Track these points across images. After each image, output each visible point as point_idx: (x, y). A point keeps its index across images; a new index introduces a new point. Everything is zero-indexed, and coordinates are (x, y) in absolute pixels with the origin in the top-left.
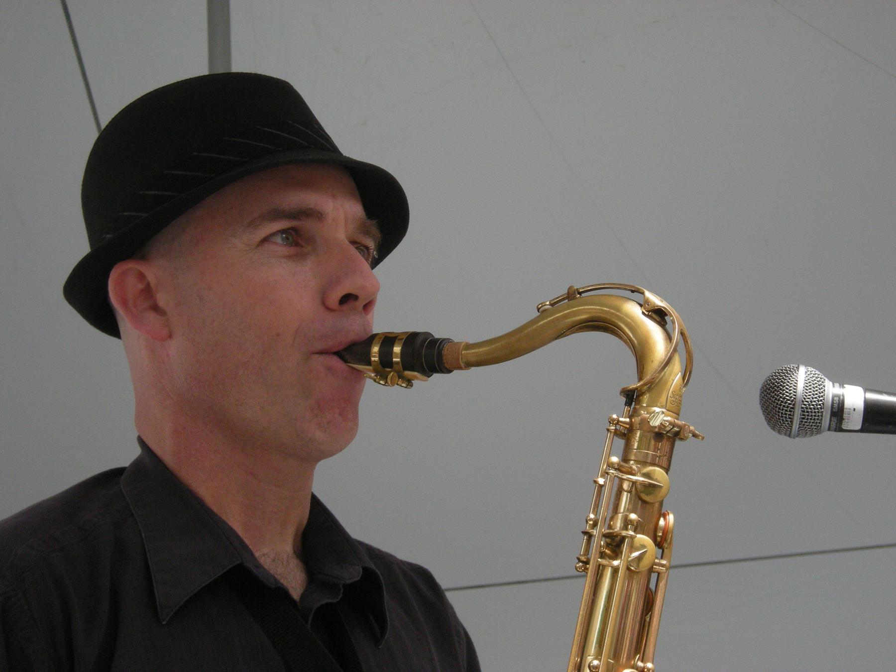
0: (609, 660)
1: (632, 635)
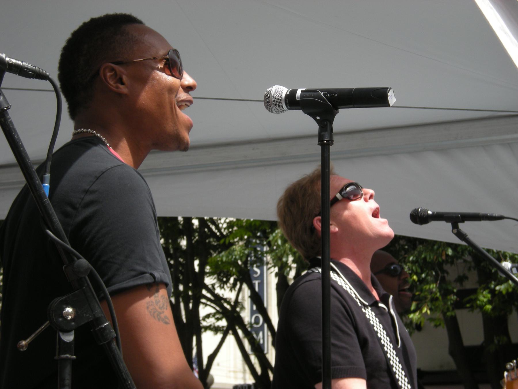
0: (63, 356)
1: (346, 319)
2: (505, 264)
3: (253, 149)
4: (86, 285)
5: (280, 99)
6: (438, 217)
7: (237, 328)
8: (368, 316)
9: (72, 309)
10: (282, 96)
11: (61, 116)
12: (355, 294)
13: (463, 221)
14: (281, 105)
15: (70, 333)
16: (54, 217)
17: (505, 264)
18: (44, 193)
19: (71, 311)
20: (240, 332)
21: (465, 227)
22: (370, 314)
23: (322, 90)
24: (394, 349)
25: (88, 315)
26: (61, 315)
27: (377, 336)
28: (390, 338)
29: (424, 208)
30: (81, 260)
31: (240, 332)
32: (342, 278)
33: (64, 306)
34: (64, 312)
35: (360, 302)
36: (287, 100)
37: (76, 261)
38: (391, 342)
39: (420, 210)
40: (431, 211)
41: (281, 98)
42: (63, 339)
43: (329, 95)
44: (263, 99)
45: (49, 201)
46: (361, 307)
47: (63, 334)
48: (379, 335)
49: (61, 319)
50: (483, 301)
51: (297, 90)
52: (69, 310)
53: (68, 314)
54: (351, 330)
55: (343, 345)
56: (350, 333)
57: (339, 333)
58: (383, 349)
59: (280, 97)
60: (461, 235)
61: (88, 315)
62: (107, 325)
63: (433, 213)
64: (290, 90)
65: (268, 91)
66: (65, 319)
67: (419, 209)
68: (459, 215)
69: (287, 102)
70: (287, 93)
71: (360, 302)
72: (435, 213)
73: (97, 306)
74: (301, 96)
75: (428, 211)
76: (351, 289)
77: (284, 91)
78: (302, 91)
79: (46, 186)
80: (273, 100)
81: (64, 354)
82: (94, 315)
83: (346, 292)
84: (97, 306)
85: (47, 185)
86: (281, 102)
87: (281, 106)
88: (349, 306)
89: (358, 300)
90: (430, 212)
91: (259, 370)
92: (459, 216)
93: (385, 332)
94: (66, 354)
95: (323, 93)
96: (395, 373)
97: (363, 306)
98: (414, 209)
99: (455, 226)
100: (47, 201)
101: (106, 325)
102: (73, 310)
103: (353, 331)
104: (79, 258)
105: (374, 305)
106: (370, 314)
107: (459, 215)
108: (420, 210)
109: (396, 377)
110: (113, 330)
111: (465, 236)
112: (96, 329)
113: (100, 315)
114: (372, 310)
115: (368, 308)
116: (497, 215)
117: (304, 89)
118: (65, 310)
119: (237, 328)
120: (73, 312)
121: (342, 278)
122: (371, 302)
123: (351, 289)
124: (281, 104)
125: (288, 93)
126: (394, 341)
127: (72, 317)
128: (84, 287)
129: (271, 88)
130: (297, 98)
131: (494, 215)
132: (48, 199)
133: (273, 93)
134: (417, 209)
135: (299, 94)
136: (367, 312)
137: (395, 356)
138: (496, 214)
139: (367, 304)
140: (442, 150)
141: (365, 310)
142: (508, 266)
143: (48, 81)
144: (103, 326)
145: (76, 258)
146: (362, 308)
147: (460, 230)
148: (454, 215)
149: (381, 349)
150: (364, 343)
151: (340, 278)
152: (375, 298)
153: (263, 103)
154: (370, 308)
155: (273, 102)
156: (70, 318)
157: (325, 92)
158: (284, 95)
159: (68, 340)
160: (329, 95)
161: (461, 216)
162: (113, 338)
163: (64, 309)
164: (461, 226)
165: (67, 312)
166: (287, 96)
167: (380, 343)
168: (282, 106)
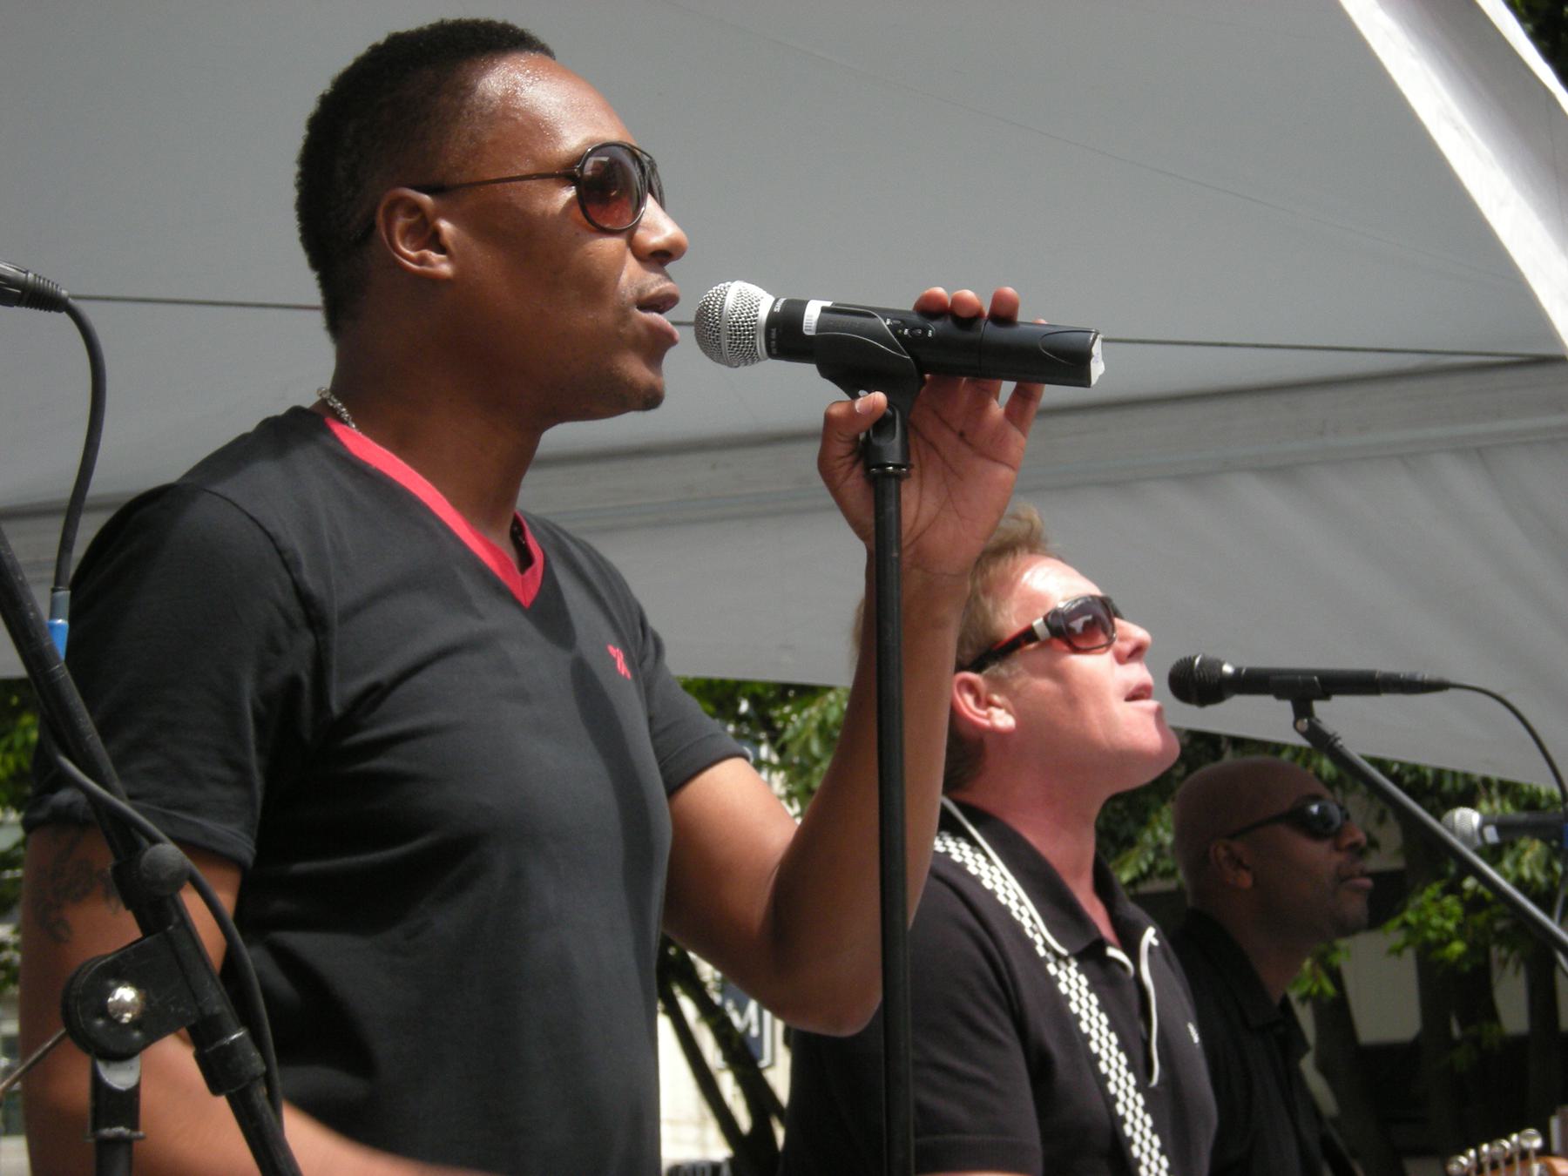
0: (107, 1132)
2: (1462, 816)
3: (714, 467)
4: (176, 919)
5: (752, 326)
6: (1253, 682)
7: (677, 990)
8: (1063, 988)
9: (133, 989)
10: (757, 315)
11: (102, 420)
12: (1031, 918)
13: (1326, 696)
14: (752, 343)
15: (127, 1064)
16: (81, 720)
17: (1462, 816)
18: (52, 648)
19: (133, 1000)
20: (688, 1007)
21: (1333, 713)
22: (1073, 983)
23: (885, 313)
24: (1138, 1089)
25: (181, 1009)
26: (103, 1011)
27: (1089, 1050)
28: (1128, 1056)
29: (1212, 654)
30: (160, 846)
31: (688, 1007)
32: (985, 854)
33: (112, 983)
34: (110, 1000)
35: (1047, 946)
36: (774, 330)
37: (146, 850)
38: (1129, 1068)
39: (1197, 661)
40: (1231, 663)
41: (755, 321)
42: (107, 1080)
43: (906, 331)
44: (692, 319)
45: (67, 672)
46: (1045, 958)
47: (107, 1065)
48: (1094, 1047)
49: (100, 1022)
50: (1442, 929)
51: (807, 302)
52: (126, 994)
53: (123, 1006)
54: (1003, 1029)
55: (977, 1071)
56: (1000, 1034)
57: (963, 1032)
58: (1104, 1090)
59: (746, 315)
60: (1322, 741)
61: (181, 1009)
62: (240, 1038)
63: (1238, 671)
64: (782, 300)
65: (711, 295)
66: (114, 1022)
67: (1195, 658)
68: (1316, 678)
69: (774, 335)
70: (775, 310)
71: (1047, 946)
72: (1244, 671)
73: (209, 983)
74: (821, 326)
75: (1221, 664)
76: (1020, 903)
77: (765, 304)
78: (824, 310)
79: (59, 625)
80: (730, 326)
81: (111, 1126)
82: (200, 1009)
83: (1005, 910)
84: (209, 983)
85: (60, 621)
86: (752, 343)
87: (751, 347)
88: (1008, 964)
89: (1038, 939)
90: (1228, 669)
91: (744, 1122)
92: (1315, 682)
93: (1113, 1037)
94: (114, 1126)
95: (888, 322)
96: (1131, 1141)
97: (1050, 956)
98: (1185, 659)
99: (1303, 710)
100: (61, 671)
101: (235, 1039)
102: (138, 995)
103: (1012, 1031)
104: (154, 840)
105: (1091, 957)
106: (1073, 983)
107: (1316, 678)
108: (1197, 661)
109: (1130, 1153)
110: (255, 1054)
111: (1332, 740)
112: (207, 1051)
113: (217, 1009)
114: (1079, 970)
115: (1068, 965)
116: (1426, 677)
117: (828, 304)
118: (113, 996)
119: (677, 990)
120: (137, 1000)
121: (985, 854)
122: (1082, 945)
123: (1020, 903)
124: (753, 339)
125: (777, 309)
126: (1140, 1066)
127: (133, 1016)
128: (171, 928)
129: (714, 291)
130: (804, 328)
131: (1419, 677)
132: (63, 664)
133: (730, 302)
134: (1190, 658)
135: (812, 316)
136: (1062, 975)
137: (1140, 1112)
138: (1427, 674)
139: (1063, 951)
140: (1281, 471)
141: (1059, 968)
142: (1471, 822)
143: (64, 314)
144: (226, 1042)
145: (145, 842)
146: (1048, 962)
147: (1318, 721)
148: (1300, 677)
149: (1096, 1089)
150: (1041, 1068)
151: (980, 857)
152: (1098, 931)
153: (693, 328)
154: (1074, 964)
155: (731, 330)
156: (127, 1016)
157: (894, 321)
158: (763, 315)
159: (121, 1085)
160: (906, 331)
161: (1319, 678)
162: (255, 1078)
163: (110, 992)
164: (1319, 707)
165: (119, 1001)
166: (773, 319)
167: (1096, 1070)
168: (755, 348)
